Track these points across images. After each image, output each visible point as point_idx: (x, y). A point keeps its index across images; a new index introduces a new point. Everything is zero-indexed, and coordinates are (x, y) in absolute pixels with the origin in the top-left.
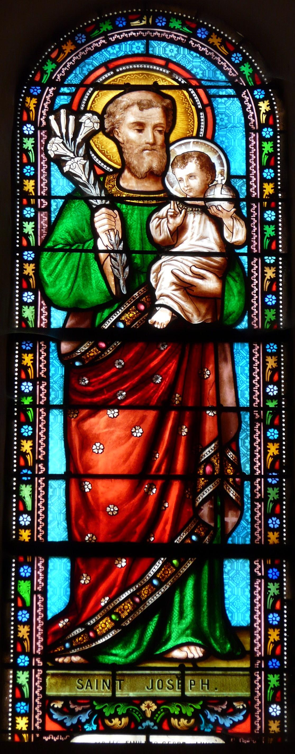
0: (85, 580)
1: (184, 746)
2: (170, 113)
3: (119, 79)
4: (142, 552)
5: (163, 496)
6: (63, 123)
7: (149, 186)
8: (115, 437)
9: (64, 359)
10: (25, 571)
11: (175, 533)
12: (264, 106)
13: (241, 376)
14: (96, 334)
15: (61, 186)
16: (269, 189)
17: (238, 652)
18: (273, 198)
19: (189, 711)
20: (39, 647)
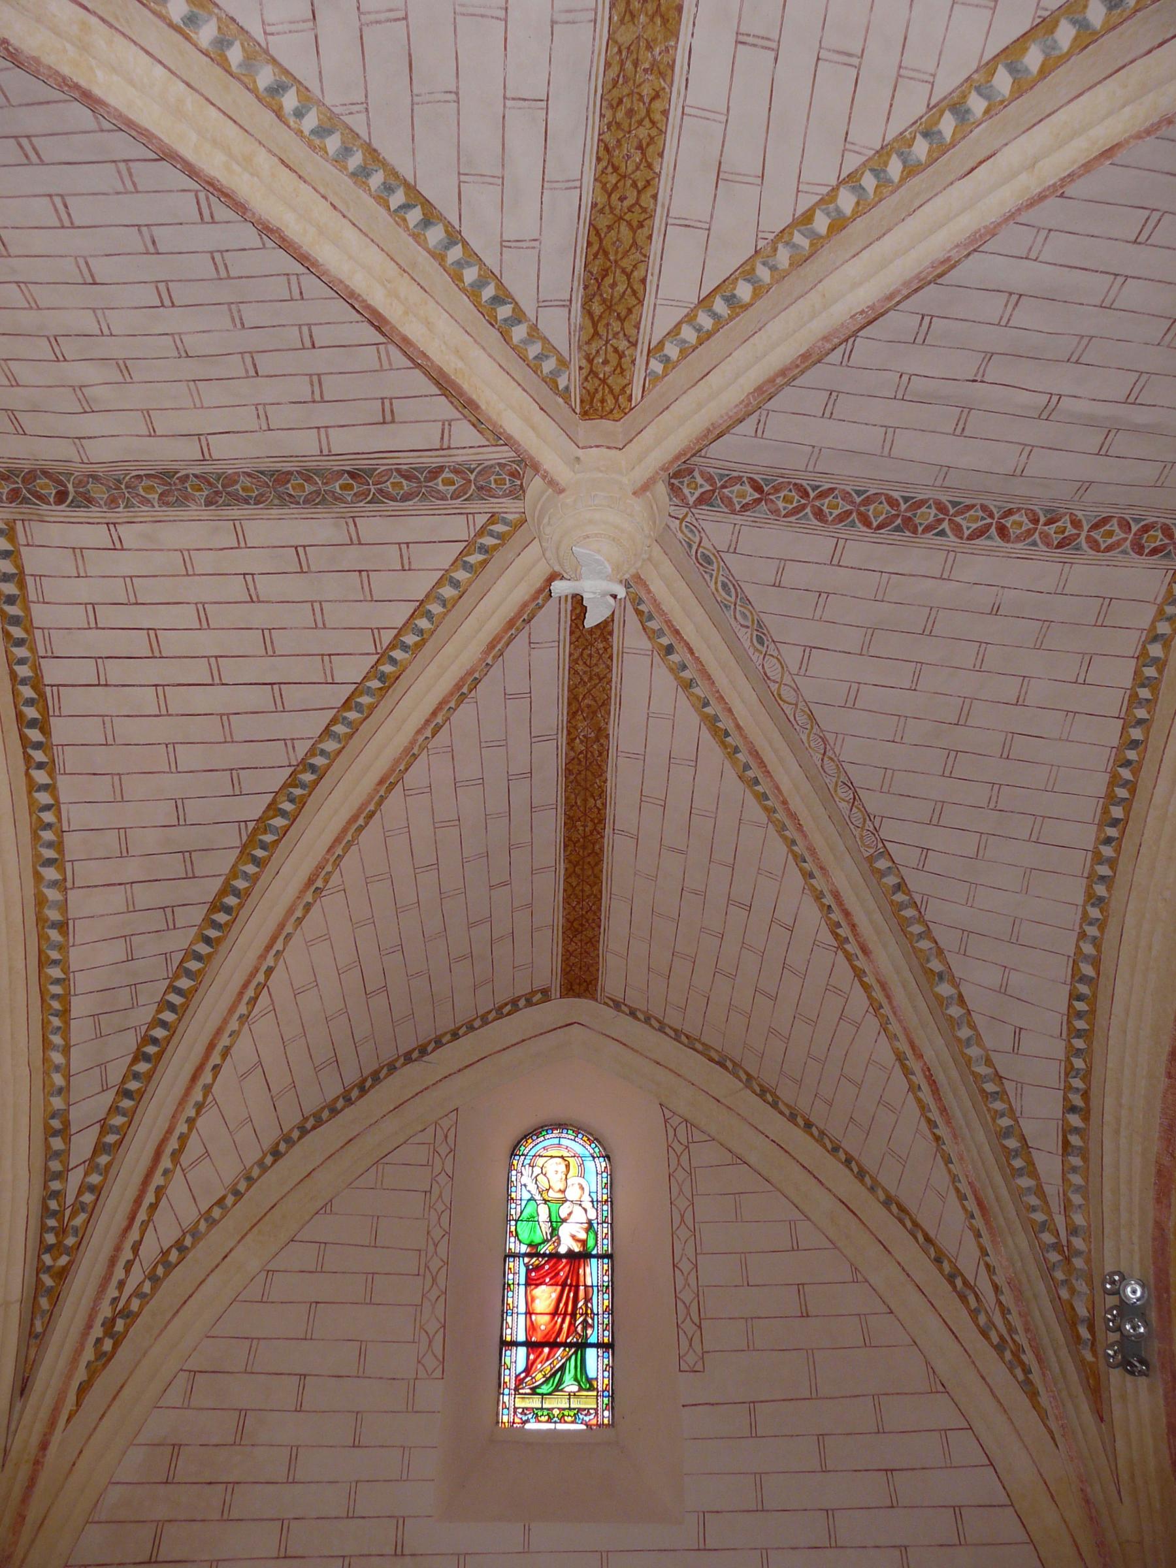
0: (532, 1357)
1: (569, 1431)
2: (568, 1166)
3: (549, 1153)
4: (554, 1345)
5: (563, 1322)
6: (527, 1171)
7: (560, 1195)
8: (545, 1297)
9: (526, 1265)
10: (508, 1353)
11: (567, 1337)
12: (604, 1164)
13: (593, 1273)
14: (538, 1255)
15: (526, 1196)
16: (605, 1197)
17: (591, 1388)
18: (606, 1201)
19: (572, 1413)
20: (513, 1386)
